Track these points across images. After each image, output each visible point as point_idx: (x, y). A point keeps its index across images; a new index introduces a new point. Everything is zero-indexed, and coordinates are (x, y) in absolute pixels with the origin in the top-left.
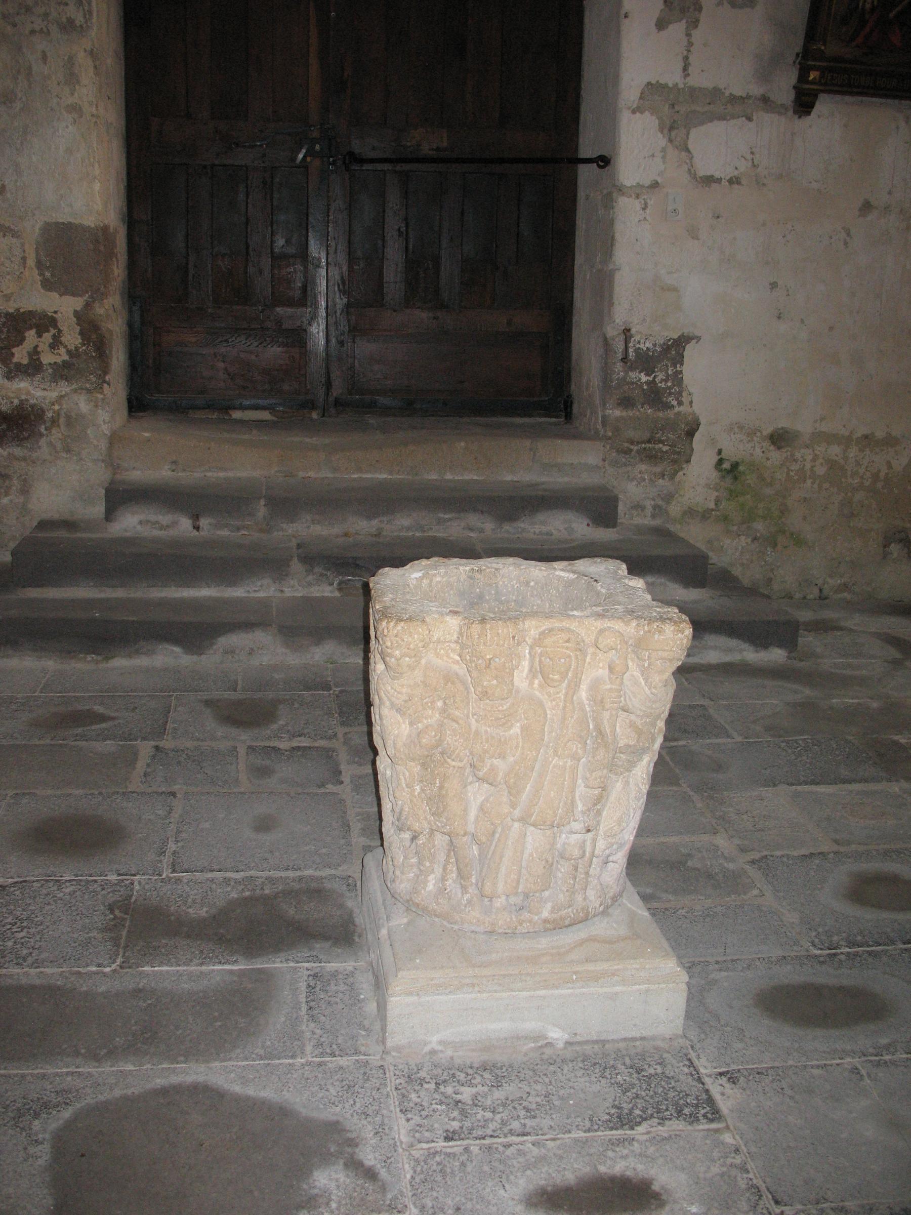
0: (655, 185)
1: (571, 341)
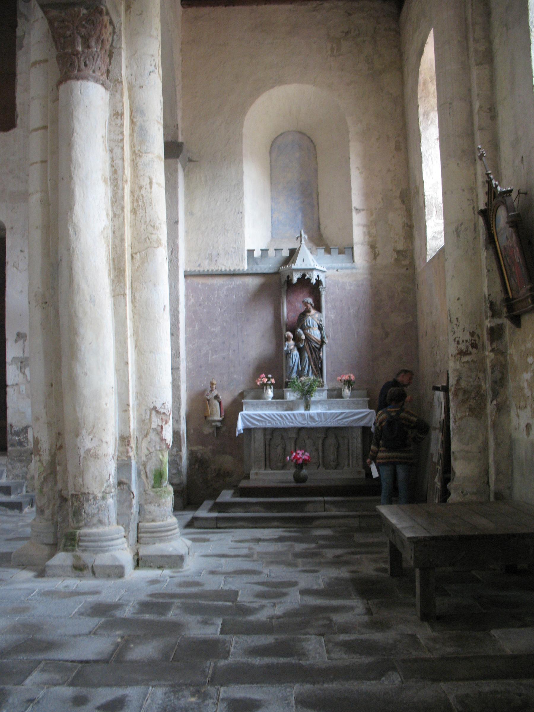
0: (17, 384)
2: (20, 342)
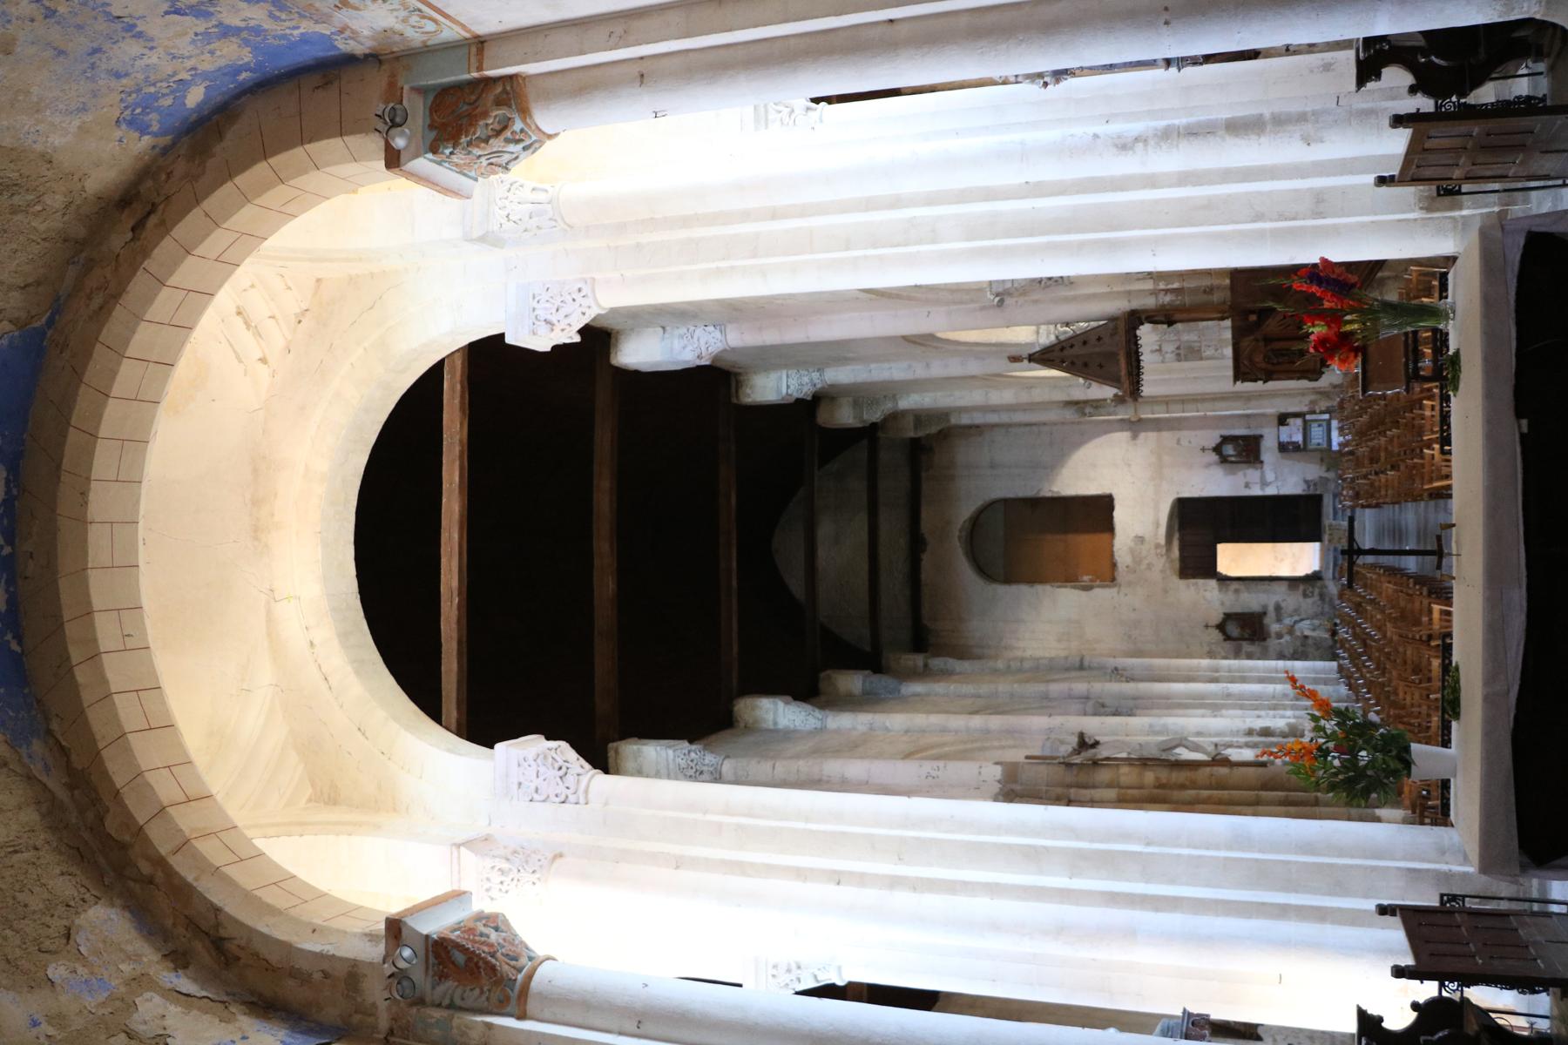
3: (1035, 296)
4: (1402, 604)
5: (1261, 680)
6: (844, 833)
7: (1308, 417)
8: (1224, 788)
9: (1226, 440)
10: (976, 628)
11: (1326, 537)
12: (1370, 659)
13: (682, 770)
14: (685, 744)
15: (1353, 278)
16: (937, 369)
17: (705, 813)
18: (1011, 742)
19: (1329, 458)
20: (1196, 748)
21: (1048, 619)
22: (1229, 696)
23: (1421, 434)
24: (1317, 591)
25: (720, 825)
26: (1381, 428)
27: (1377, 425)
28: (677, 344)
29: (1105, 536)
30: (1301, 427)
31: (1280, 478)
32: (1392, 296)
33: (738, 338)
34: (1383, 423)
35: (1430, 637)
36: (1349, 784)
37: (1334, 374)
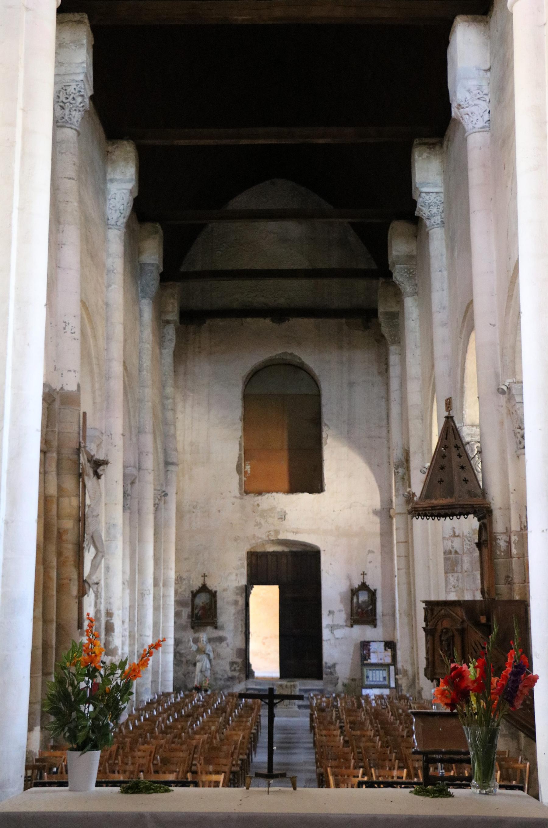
0: (329, 640)
1: (39, 492)
2: (331, 616)
3: (507, 423)
4: (225, 748)
5: (156, 624)
6: (10, 243)
7: (392, 668)
8: (58, 592)
9: (373, 594)
10: (202, 368)
11: (284, 682)
12: (175, 720)
13: (64, 88)
14: (90, 92)
15: (518, 705)
16: (441, 334)
17: (23, 110)
18: (98, 400)
19: (356, 685)
20: (95, 566)
21: (210, 432)
22: (142, 595)
23: (376, 766)
24: (236, 674)
25: (12, 124)
26: (382, 732)
27: (385, 728)
28: (472, 84)
29: (286, 487)
30: (383, 660)
31: (337, 641)
32: (502, 744)
33: (476, 143)
34: (386, 734)
35: (195, 773)
36: (64, 696)
37: (429, 689)
